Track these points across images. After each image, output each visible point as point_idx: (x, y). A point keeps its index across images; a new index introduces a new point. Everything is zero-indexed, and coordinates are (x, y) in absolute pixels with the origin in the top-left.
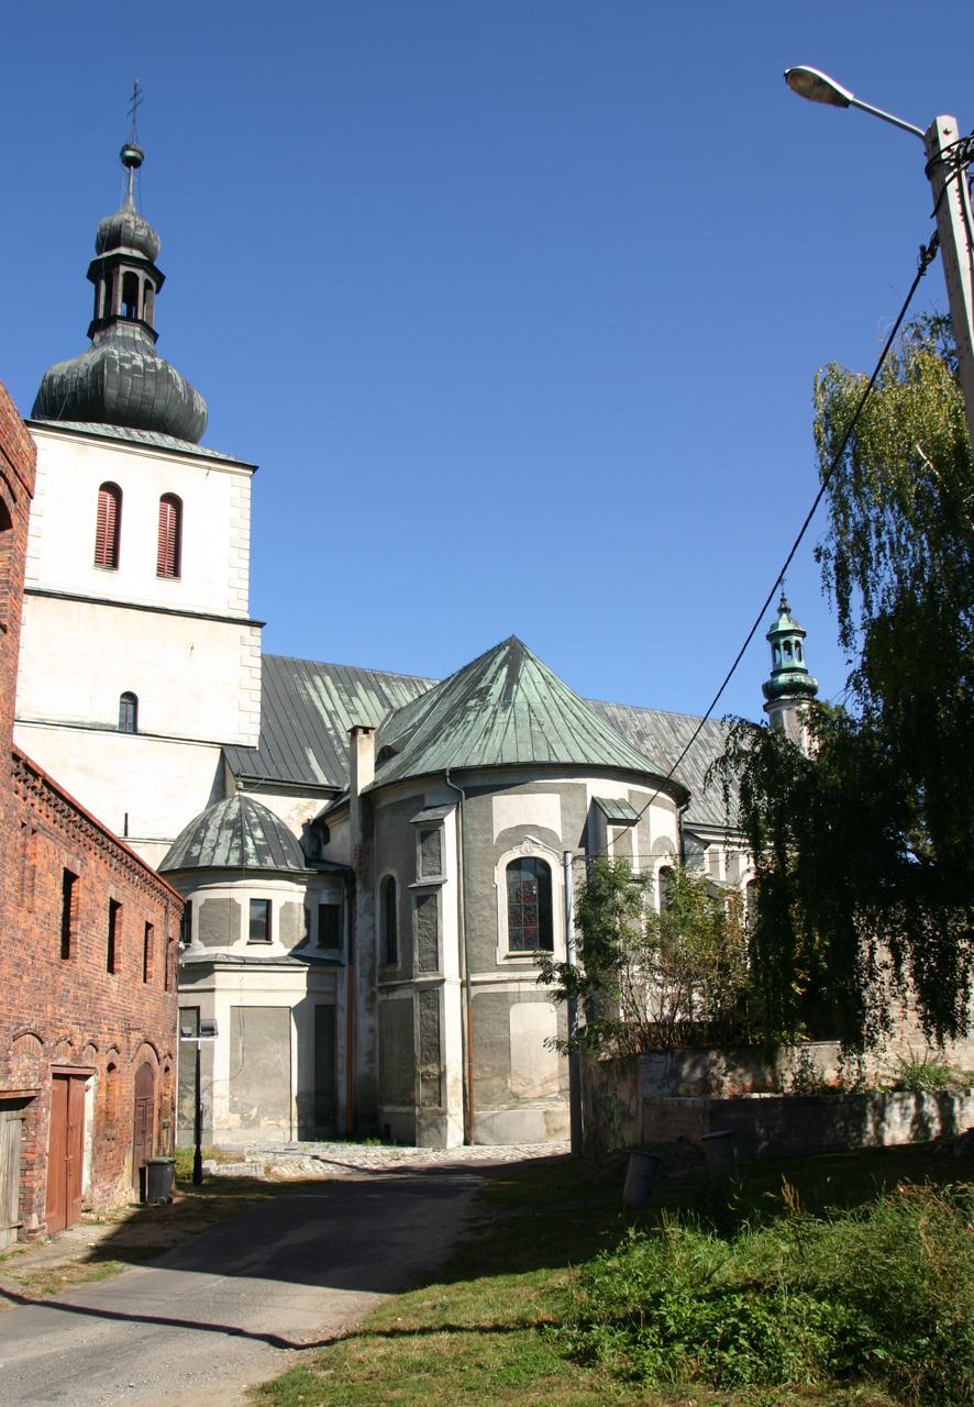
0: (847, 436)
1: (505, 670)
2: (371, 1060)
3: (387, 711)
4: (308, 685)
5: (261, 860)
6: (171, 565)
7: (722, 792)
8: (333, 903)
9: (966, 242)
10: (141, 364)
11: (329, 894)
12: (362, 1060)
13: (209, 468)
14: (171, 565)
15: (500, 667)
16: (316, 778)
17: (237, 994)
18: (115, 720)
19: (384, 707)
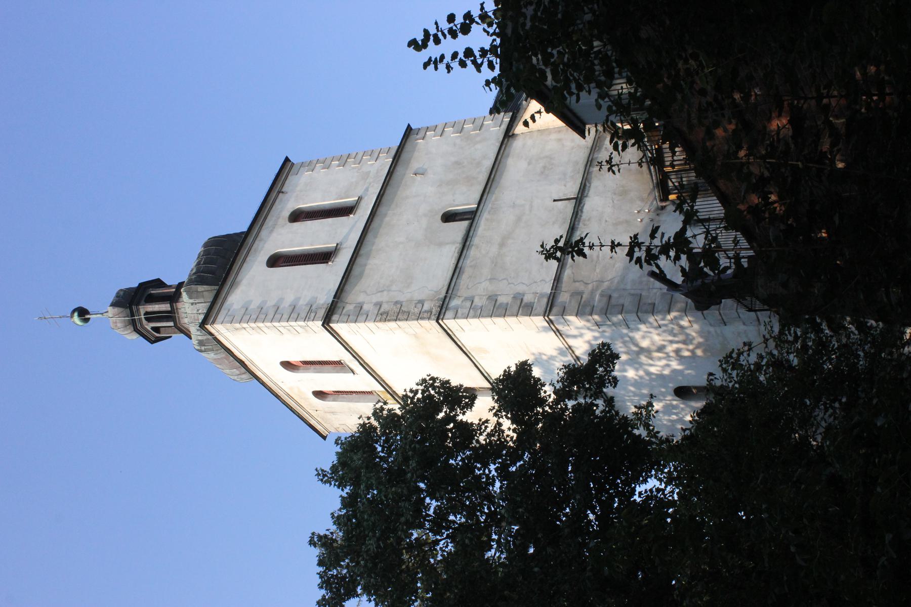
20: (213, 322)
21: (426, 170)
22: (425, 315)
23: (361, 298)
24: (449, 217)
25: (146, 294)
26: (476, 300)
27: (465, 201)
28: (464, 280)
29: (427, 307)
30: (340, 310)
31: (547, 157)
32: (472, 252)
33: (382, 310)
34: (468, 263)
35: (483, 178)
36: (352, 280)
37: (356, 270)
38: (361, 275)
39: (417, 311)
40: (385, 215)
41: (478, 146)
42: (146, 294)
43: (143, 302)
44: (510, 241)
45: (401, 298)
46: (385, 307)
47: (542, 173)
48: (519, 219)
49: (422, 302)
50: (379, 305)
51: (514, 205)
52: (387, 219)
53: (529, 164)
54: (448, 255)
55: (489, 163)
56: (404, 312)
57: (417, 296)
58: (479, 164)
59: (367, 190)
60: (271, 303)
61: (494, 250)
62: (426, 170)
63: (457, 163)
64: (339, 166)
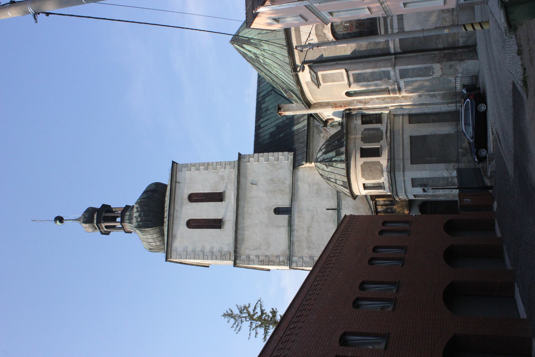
0: (322, 55)
1: (245, 46)
2: (435, 96)
3: (273, 92)
4: (265, 129)
5: (342, 154)
6: (218, 197)
7: (300, 317)
8: (360, 118)
9: (325, 56)
10: (138, 214)
11: (356, 120)
12: (435, 100)
13: (176, 182)
14: (218, 197)
15: (244, 48)
16: (304, 127)
17: (405, 160)
18: (286, 217)
19: (271, 94)
20: (171, 257)
21: (257, 182)
22: (282, 263)
23: (247, 252)
24: (278, 211)
25: (102, 217)
26: (304, 258)
27: (284, 202)
28: (296, 248)
29: (281, 259)
30: (239, 258)
31: (316, 184)
32: (295, 233)
33: (260, 259)
34: (295, 239)
35: (288, 190)
36: (239, 242)
37: (239, 237)
38: (243, 240)
39: (277, 261)
40: (244, 207)
41: (280, 171)
42: (102, 217)
43: (102, 221)
44: (312, 229)
45: (269, 253)
46: (261, 258)
47: (317, 193)
48: (313, 218)
49: (278, 256)
50: (258, 256)
51: (308, 210)
52: (246, 209)
53: (309, 186)
54: (283, 232)
55: (289, 182)
56: (271, 261)
57: (276, 254)
58: (283, 183)
59: (226, 187)
60: (199, 249)
61: (305, 233)
62: (257, 182)
63: (272, 180)
64: (205, 170)
